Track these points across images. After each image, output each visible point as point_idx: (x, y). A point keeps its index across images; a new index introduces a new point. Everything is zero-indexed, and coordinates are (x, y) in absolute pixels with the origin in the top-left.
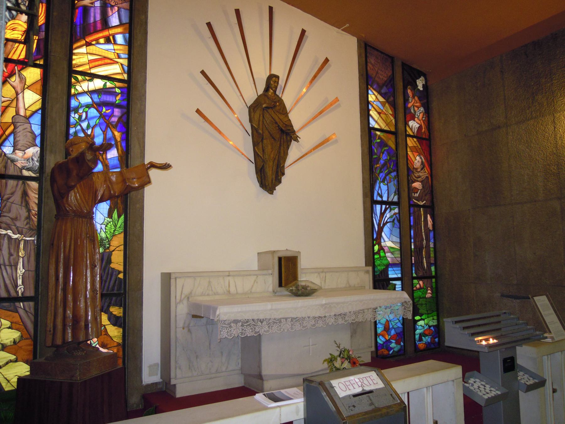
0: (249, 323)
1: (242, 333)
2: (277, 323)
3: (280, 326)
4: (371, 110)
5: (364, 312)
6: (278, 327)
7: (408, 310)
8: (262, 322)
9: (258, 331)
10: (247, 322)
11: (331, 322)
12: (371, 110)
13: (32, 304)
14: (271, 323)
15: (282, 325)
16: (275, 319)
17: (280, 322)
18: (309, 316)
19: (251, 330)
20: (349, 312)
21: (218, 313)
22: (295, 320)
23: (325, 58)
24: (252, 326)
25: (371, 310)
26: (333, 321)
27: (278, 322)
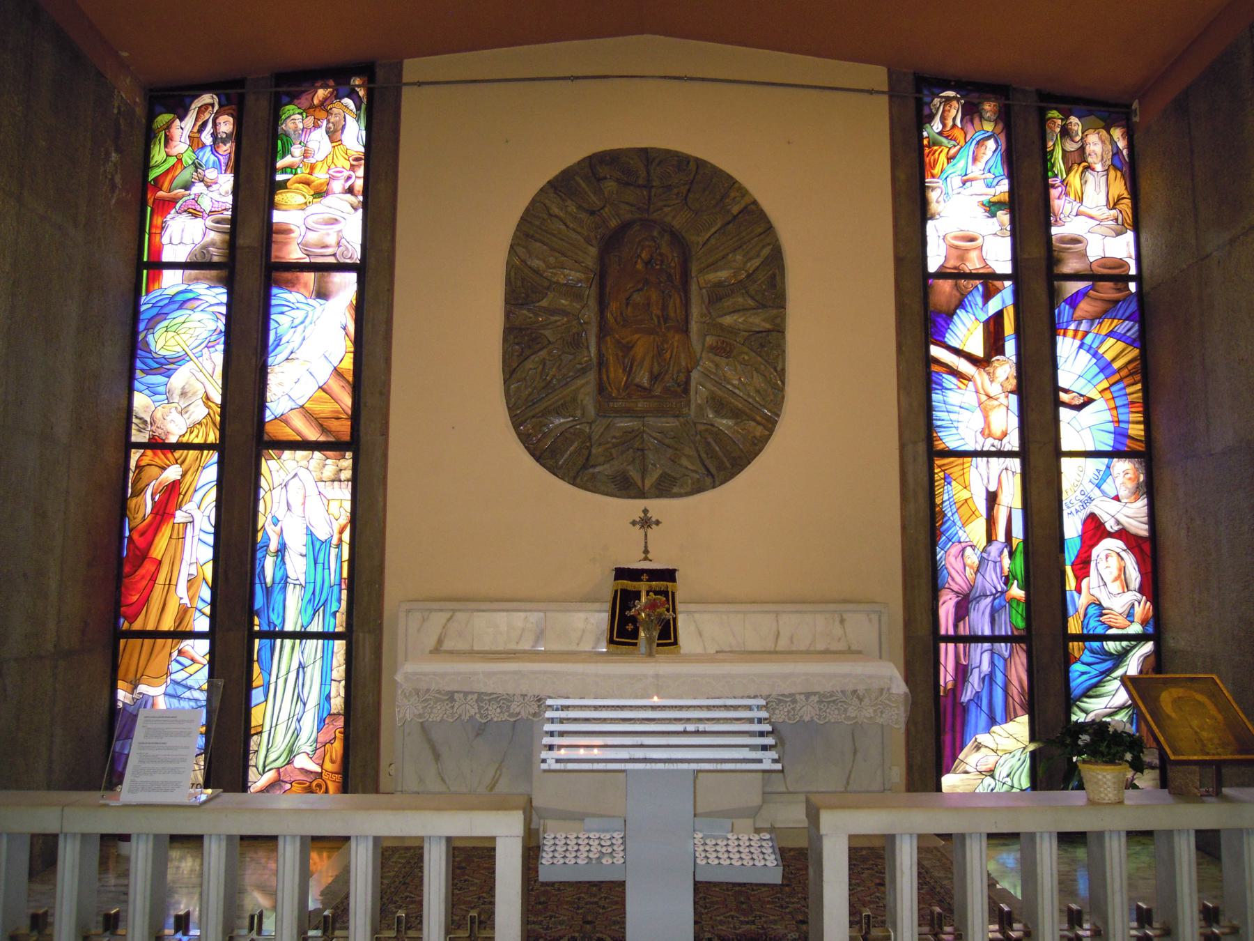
0: (834, 698)
1: (820, 716)
2: (443, 701)
3: (793, 709)
4: (382, 848)
5: (794, 701)
6: (789, 712)
7: (829, 702)
8: (861, 700)
9: (853, 715)
10: (831, 696)
11: (809, 716)
12: (382, 848)
13: (134, 439)
14: (772, 702)
15: (456, 706)
16: (439, 692)
17: (452, 699)
18: (524, 693)
19: (498, 710)
20: (522, 695)
21: (1114, 652)
22: (487, 698)
23: (349, 835)
24: (840, 704)
25: (816, 699)
26: (813, 714)
27: (788, 700)
